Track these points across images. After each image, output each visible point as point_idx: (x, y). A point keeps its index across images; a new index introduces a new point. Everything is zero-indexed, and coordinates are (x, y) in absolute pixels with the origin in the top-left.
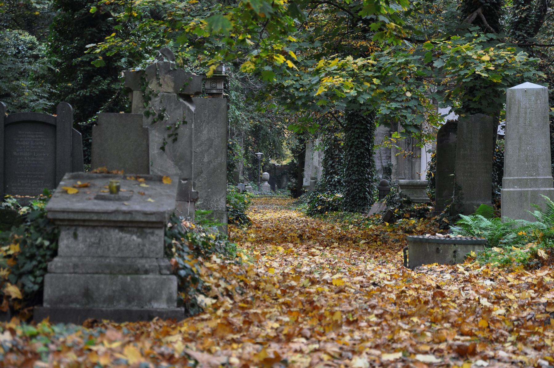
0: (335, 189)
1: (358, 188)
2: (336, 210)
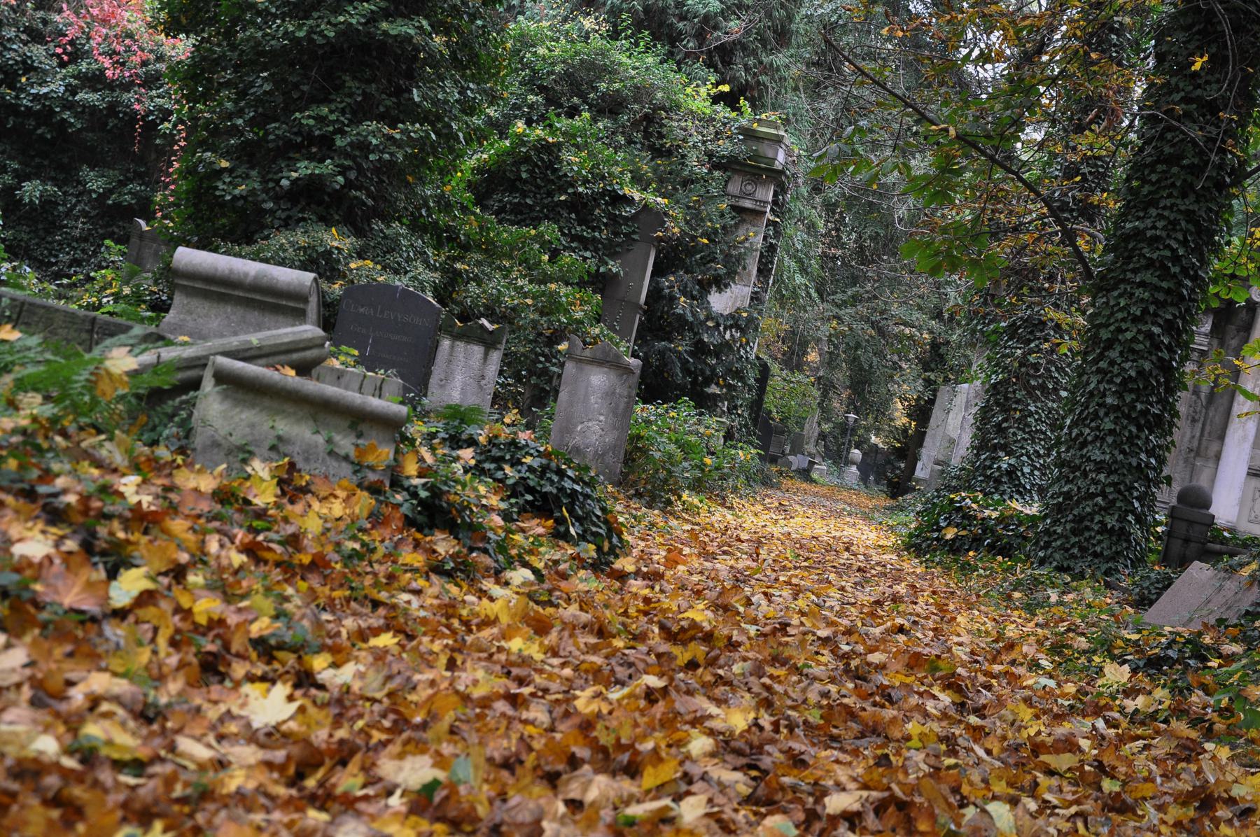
0: (997, 489)
1: (1103, 494)
2: (1006, 551)
